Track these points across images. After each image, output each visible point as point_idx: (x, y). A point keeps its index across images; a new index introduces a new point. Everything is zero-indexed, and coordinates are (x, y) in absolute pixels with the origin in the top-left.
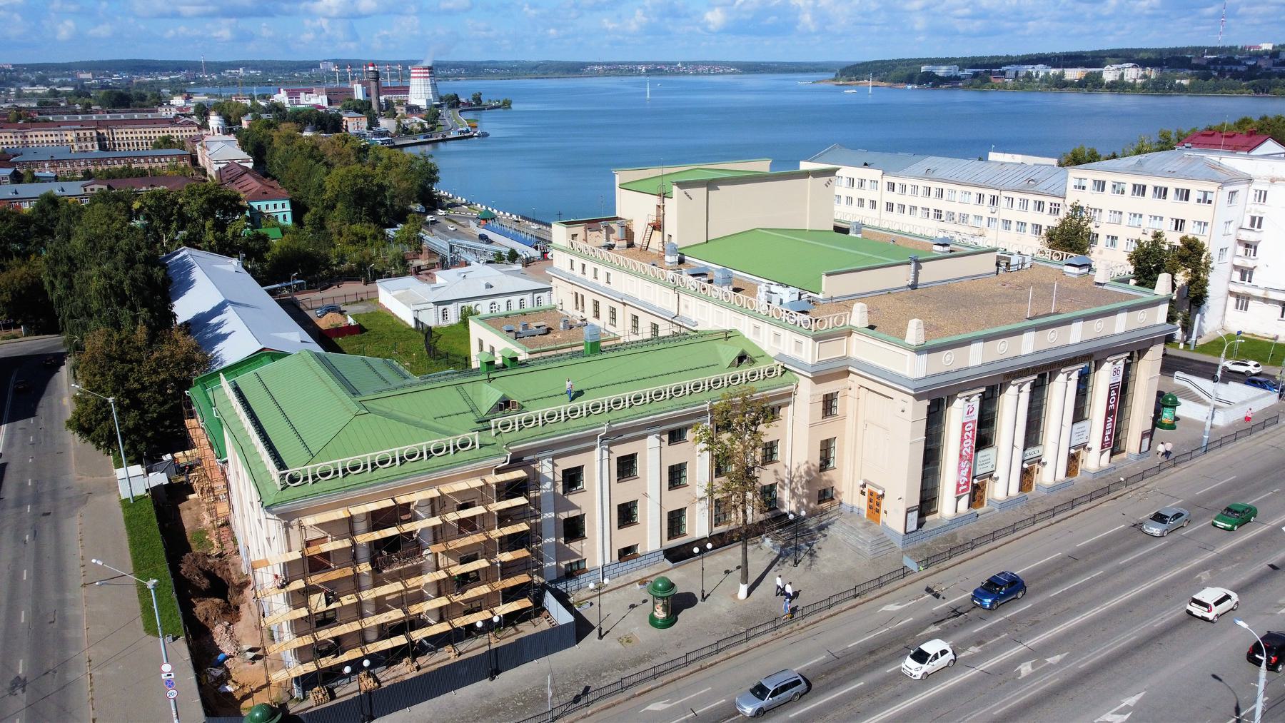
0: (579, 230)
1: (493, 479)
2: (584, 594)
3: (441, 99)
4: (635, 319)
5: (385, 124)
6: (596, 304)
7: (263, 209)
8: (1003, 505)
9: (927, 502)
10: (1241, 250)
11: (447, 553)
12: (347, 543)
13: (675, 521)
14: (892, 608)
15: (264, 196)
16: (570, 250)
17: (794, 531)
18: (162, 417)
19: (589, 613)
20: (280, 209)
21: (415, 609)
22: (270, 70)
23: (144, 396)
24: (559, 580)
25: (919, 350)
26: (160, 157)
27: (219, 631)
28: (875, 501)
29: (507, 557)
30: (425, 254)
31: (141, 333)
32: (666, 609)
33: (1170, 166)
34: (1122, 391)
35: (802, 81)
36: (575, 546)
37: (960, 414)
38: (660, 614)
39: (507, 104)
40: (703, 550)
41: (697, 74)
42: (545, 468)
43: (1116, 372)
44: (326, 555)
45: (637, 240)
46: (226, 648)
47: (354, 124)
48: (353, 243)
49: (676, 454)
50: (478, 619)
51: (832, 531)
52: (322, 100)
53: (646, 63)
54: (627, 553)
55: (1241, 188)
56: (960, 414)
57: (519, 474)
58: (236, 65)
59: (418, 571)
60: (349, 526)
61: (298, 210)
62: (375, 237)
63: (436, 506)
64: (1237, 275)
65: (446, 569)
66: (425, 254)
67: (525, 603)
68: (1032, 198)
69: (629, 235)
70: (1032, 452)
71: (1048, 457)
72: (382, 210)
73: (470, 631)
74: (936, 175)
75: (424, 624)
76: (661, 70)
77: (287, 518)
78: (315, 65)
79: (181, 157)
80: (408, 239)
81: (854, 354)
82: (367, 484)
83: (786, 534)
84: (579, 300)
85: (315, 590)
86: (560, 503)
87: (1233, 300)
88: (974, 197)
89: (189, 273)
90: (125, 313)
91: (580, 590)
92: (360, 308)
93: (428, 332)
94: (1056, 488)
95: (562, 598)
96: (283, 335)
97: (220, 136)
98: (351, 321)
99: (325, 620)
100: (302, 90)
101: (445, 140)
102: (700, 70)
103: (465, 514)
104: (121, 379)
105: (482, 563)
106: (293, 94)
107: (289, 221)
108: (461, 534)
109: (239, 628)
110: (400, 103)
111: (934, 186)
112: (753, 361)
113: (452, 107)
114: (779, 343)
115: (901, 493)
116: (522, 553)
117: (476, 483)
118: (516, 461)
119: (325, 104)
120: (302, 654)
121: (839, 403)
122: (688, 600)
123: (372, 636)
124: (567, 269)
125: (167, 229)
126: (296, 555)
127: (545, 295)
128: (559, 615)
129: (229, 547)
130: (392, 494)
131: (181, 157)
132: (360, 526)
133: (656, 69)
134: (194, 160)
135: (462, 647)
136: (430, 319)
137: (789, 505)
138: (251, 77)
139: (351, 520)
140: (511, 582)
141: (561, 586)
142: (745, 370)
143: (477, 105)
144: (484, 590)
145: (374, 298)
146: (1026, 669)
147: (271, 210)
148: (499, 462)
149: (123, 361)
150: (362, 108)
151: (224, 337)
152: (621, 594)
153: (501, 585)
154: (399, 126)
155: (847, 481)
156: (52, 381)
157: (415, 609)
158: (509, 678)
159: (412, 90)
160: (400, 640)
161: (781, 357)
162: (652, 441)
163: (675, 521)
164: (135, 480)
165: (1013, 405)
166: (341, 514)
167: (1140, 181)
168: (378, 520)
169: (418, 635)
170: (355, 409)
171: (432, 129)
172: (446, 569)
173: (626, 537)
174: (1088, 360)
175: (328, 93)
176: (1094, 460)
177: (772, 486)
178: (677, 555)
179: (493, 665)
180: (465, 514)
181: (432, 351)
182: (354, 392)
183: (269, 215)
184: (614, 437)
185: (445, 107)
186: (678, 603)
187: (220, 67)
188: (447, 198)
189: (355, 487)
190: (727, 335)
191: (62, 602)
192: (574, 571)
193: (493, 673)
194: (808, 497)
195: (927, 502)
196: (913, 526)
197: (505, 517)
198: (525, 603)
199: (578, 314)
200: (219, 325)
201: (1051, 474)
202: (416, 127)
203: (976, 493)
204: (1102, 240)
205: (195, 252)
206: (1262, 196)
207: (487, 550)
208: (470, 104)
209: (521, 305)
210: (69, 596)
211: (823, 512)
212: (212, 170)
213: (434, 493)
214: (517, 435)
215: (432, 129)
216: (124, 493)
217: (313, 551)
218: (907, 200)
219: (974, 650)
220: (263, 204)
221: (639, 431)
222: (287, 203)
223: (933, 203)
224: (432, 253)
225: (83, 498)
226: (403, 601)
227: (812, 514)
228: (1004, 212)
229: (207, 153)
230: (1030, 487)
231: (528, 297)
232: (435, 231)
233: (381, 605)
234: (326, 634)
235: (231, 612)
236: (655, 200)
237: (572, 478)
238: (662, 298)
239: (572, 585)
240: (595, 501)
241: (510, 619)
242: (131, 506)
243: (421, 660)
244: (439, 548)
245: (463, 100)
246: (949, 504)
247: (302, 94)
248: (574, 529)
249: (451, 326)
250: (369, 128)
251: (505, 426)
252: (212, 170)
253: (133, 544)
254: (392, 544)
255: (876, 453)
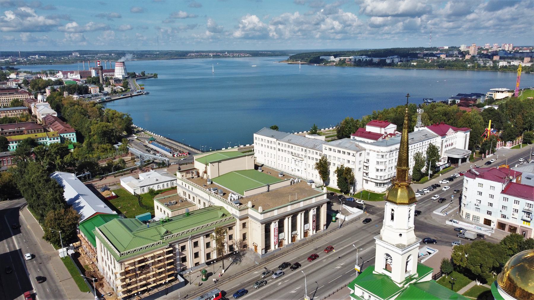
0: (184, 174)
1: (165, 250)
2: (187, 275)
3: (128, 74)
4: (199, 200)
5: (107, 89)
6: (189, 195)
7: (65, 136)
8: (287, 246)
9: (267, 246)
10: (365, 168)
11: (155, 268)
12: (134, 267)
13: (208, 256)
14: (256, 272)
15: (65, 132)
16: (182, 180)
17: (236, 255)
18: (70, 234)
19: (188, 279)
20: (71, 136)
21: (148, 281)
22: (51, 56)
23: (65, 229)
24: (181, 271)
25: (261, 214)
26: (16, 110)
27: (100, 289)
28: (256, 247)
29: (169, 267)
30: (130, 154)
31: (62, 211)
32: (205, 276)
33: (348, 145)
34: (317, 217)
35: (274, 62)
36: (184, 263)
37: (274, 226)
38: (204, 278)
39: (155, 76)
40: (214, 263)
41: (234, 57)
42: (177, 246)
43: (314, 212)
44: (129, 270)
45: (201, 175)
46: (103, 293)
47: (93, 89)
48: (103, 152)
49: (208, 240)
50: (163, 282)
51: (246, 255)
52: (78, 77)
53: (213, 52)
54: (197, 264)
55: (363, 152)
56: (274, 226)
57: (171, 249)
58: (34, 54)
59: (149, 272)
60: (134, 264)
61: (80, 138)
62: (111, 149)
63: (153, 258)
64: (365, 174)
65: (155, 271)
66: (130, 154)
67: (173, 278)
68: (315, 151)
69: (198, 174)
70: (294, 233)
71: (299, 233)
72: (113, 138)
73: (161, 285)
74: (291, 142)
75: (150, 284)
76: (219, 55)
77: (121, 263)
78: (70, 53)
79: (25, 110)
80: (123, 150)
81: (249, 213)
82: (138, 254)
83: (235, 256)
84: (185, 193)
85: (126, 278)
86: (181, 254)
87: (364, 181)
88: (300, 150)
89: (62, 182)
90: (57, 205)
91: (186, 274)
92: (114, 188)
93: (138, 196)
94: (289, 245)
95: (182, 276)
96: (99, 206)
97: (42, 103)
98: (114, 194)
99: (129, 285)
100: (69, 72)
101: (132, 96)
102: (235, 55)
103: (159, 259)
104: (59, 224)
105: (163, 269)
106: (65, 73)
107: (75, 141)
108: (158, 263)
109: (104, 288)
110: (111, 78)
111: (290, 145)
112: (226, 215)
113: (133, 77)
114: (233, 211)
115: (261, 245)
116: (172, 266)
117: (162, 252)
118: (171, 246)
119: (79, 78)
120: (124, 293)
121: (247, 224)
122: (211, 274)
123: (139, 287)
124: (181, 184)
125: (43, 159)
126: (123, 271)
127: (175, 181)
128: (181, 280)
129: (96, 269)
130: (143, 256)
131: (25, 110)
132: (137, 263)
133: (218, 55)
134: (30, 111)
135: (159, 289)
136: (139, 192)
137: (236, 249)
138: (42, 60)
139: (134, 262)
140: (170, 273)
141: (181, 273)
142: (224, 218)
143: (143, 77)
144: (164, 275)
145: (119, 183)
146: (280, 284)
147: (68, 137)
148: (167, 247)
149: (59, 219)
150: (95, 81)
151: (82, 207)
152: (196, 274)
153: (168, 274)
154: (112, 90)
155: (250, 242)
156: (20, 221)
157: (148, 281)
158: (170, 294)
159: (116, 71)
160: (145, 288)
161: (233, 214)
162: (202, 238)
163: (208, 256)
164: (63, 252)
165: (287, 223)
166: (132, 261)
167: (339, 149)
168: (140, 262)
169: (149, 287)
170: (133, 236)
171: (126, 91)
172: (155, 271)
173: (196, 260)
174: (306, 211)
175: (80, 73)
176: (311, 233)
177: (232, 245)
178: (208, 264)
179: (166, 292)
180: (159, 259)
181: (141, 204)
182: (131, 231)
183: (68, 139)
184: (193, 238)
185: (130, 78)
186: (208, 275)
187: (26, 54)
188: (135, 128)
189: (136, 255)
190: (221, 208)
191: (56, 286)
192: (184, 269)
193: (166, 294)
194: (241, 247)
195: (267, 246)
196: (264, 253)
197: (168, 259)
198: (173, 278)
199: (184, 197)
200: (79, 203)
201: (300, 237)
202: (119, 90)
203: (280, 243)
204: (332, 164)
205: (62, 173)
206: (368, 154)
207: (164, 266)
208: (140, 76)
209: (167, 185)
210: (58, 284)
211: (245, 250)
212: (40, 117)
213: (152, 255)
214: (170, 239)
215: (126, 91)
216: (61, 256)
217: (127, 270)
218: (284, 149)
219: (271, 280)
220: (65, 135)
221: (198, 236)
222: (75, 134)
223: (291, 150)
224: (132, 154)
225: (49, 258)
226: (145, 279)
227: (242, 251)
228: (308, 155)
229: (38, 110)
230: (295, 241)
231: (169, 183)
232: (132, 144)
233: (141, 281)
234: (129, 288)
235: (102, 285)
236: (205, 166)
237: (183, 248)
238: (205, 196)
239: (184, 272)
240: (189, 253)
241: (170, 282)
242: (64, 259)
243: (150, 292)
244: (153, 267)
245: (137, 74)
246: (273, 247)
247: (69, 74)
248: (184, 259)
249: (145, 194)
250: (100, 92)
251: (167, 238)
252: (40, 117)
253: (69, 270)
254: (143, 267)
255: (256, 237)
